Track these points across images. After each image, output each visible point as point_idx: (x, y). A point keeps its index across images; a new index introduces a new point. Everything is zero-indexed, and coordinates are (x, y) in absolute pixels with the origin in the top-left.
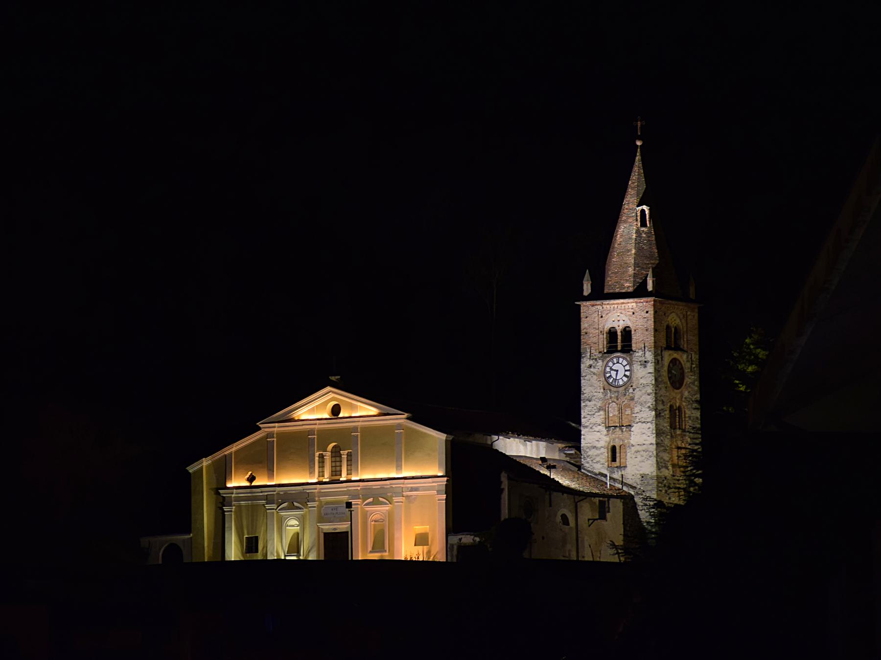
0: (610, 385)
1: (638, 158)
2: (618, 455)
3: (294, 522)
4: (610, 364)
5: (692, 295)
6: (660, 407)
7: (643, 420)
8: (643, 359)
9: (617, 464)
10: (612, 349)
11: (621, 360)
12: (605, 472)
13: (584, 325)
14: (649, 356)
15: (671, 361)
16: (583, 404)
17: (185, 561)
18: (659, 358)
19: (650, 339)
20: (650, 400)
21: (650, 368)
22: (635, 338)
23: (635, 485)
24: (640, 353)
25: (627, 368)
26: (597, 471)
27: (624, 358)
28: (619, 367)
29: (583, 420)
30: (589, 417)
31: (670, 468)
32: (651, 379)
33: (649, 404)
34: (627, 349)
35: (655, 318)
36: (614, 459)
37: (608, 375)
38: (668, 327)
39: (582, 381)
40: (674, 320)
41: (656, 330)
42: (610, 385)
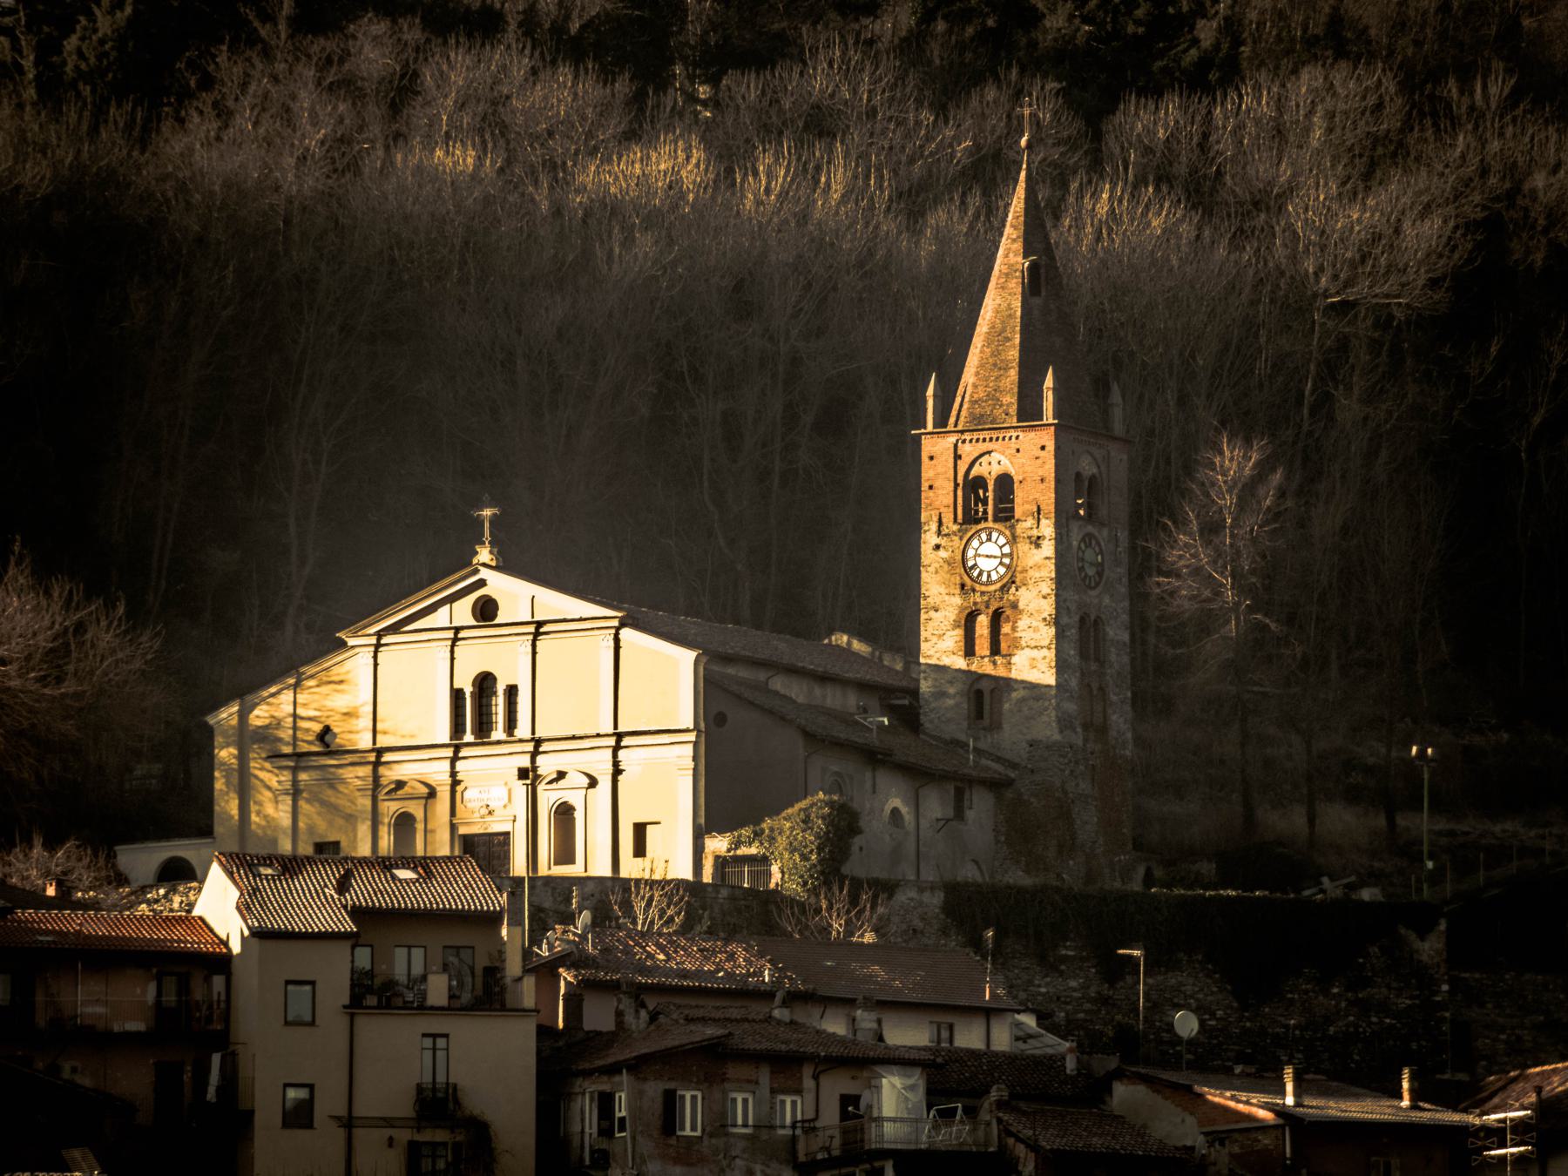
0: (966, 578)
1: (1023, 174)
2: (987, 708)
3: (985, 564)
4: (975, 543)
5: (1118, 428)
6: (1065, 620)
7: (1033, 644)
8: (1035, 533)
9: (986, 721)
10: (971, 518)
11: (995, 535)
12: (963, 737)
13: (217, 808)
14: (1047, 529)
15: (1083, 540)
16: (923, 616)
17: (689, 656)
18: (1064, 531)
19: (1048, 499)
20: (1048, 607)
21: (1048, 548)
22: (1020, 495)
23: (1017, 760)
24: (1030, 522)
25: (1007, 550)
26: (947, 737)
27: (1001, 533)
28: (988, 554)
29: (923, 646)
30: (934, 639)
31: (1079, 730)
32: (1049, 570)
33: (1045, 615)
34: (1005, 515)
35: (1056, 457)
36: (979, 715)
37: (970, 564)
38: (1078, 475)
39: (923, 575)
40: (1087, 467)
41: (1058, 481)
42: (966, 578)
